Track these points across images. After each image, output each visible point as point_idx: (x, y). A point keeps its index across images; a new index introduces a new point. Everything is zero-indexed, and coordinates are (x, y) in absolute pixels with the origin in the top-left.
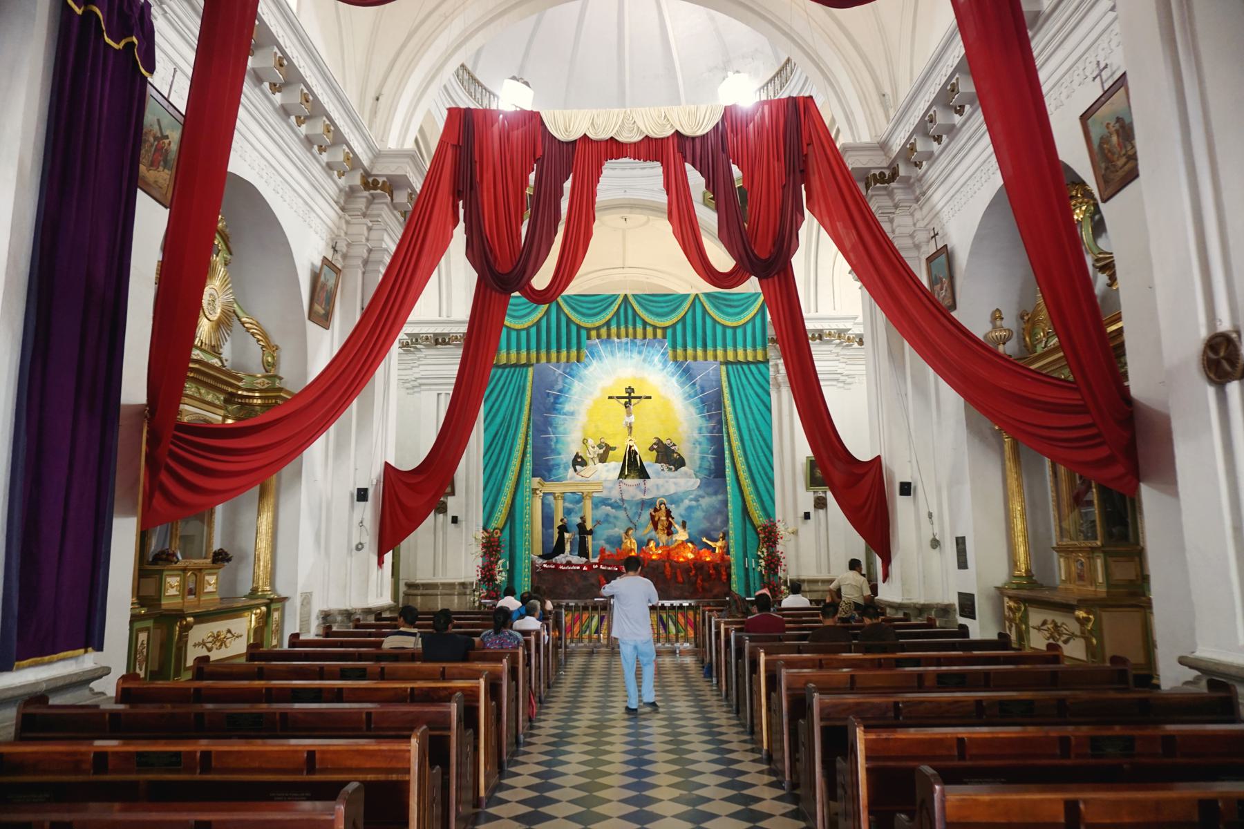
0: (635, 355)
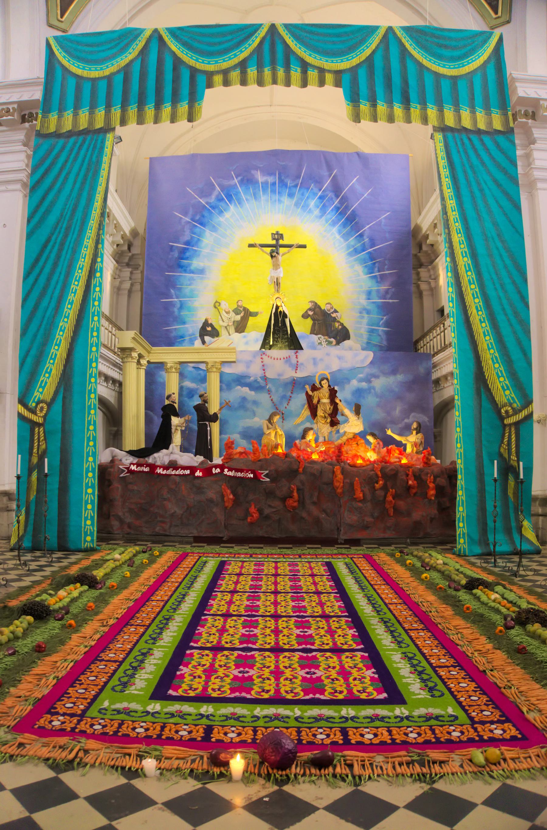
0: (286, 200)
